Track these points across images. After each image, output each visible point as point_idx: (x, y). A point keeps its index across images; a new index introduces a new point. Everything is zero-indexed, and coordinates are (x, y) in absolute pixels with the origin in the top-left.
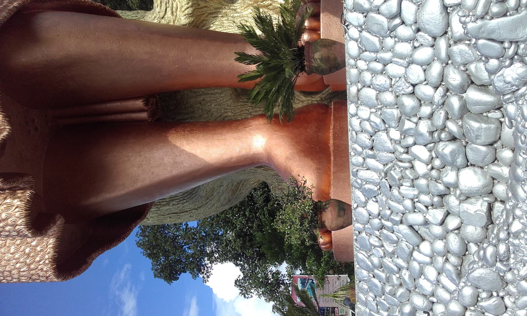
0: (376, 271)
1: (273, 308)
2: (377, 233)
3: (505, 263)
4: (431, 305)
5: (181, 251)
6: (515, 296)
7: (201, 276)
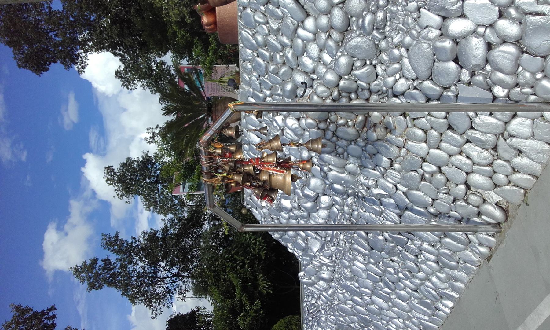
0: (261, 50)
1: (160, 100)
2: (263, 8)
3: (381, 31)
4: (311, 82)
5: (47, 39)
6: (387, 64)
7: (75, 67)
